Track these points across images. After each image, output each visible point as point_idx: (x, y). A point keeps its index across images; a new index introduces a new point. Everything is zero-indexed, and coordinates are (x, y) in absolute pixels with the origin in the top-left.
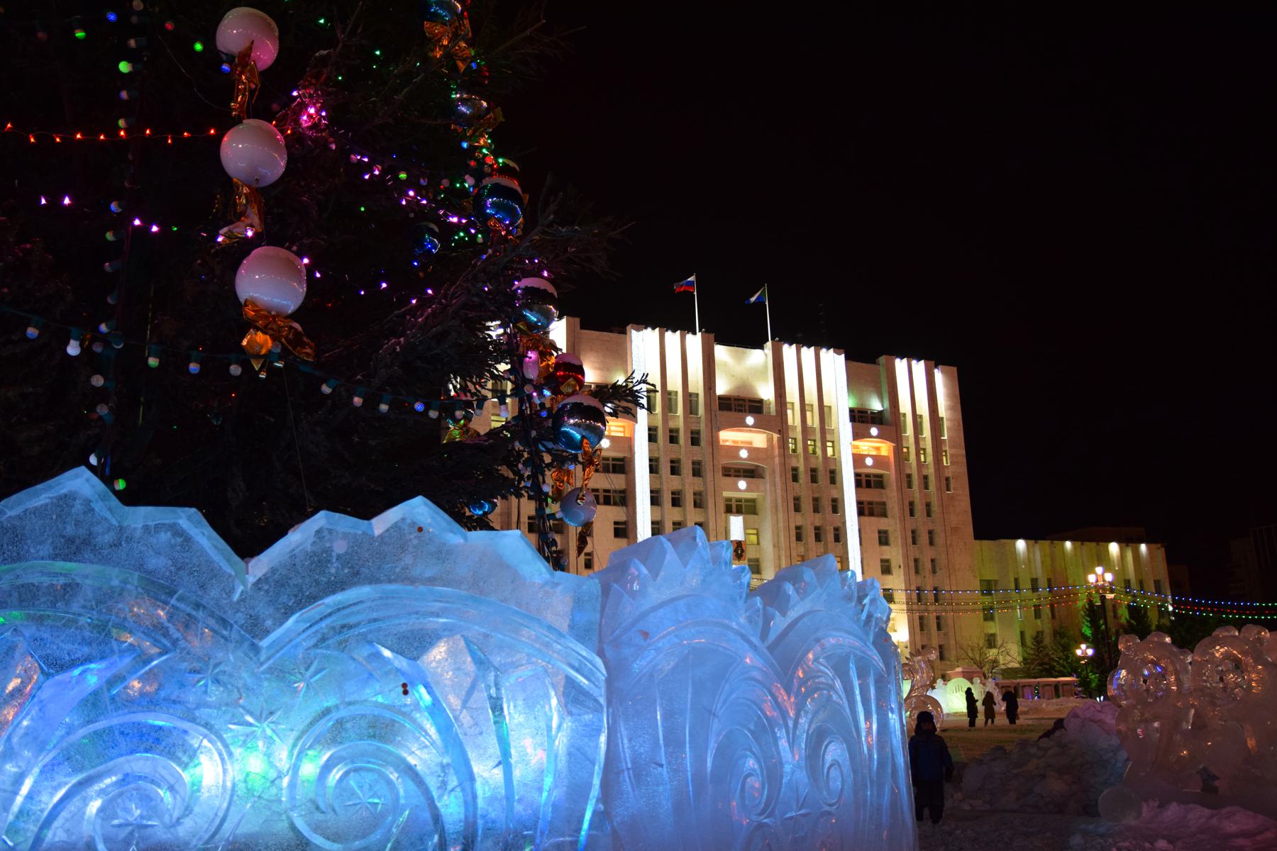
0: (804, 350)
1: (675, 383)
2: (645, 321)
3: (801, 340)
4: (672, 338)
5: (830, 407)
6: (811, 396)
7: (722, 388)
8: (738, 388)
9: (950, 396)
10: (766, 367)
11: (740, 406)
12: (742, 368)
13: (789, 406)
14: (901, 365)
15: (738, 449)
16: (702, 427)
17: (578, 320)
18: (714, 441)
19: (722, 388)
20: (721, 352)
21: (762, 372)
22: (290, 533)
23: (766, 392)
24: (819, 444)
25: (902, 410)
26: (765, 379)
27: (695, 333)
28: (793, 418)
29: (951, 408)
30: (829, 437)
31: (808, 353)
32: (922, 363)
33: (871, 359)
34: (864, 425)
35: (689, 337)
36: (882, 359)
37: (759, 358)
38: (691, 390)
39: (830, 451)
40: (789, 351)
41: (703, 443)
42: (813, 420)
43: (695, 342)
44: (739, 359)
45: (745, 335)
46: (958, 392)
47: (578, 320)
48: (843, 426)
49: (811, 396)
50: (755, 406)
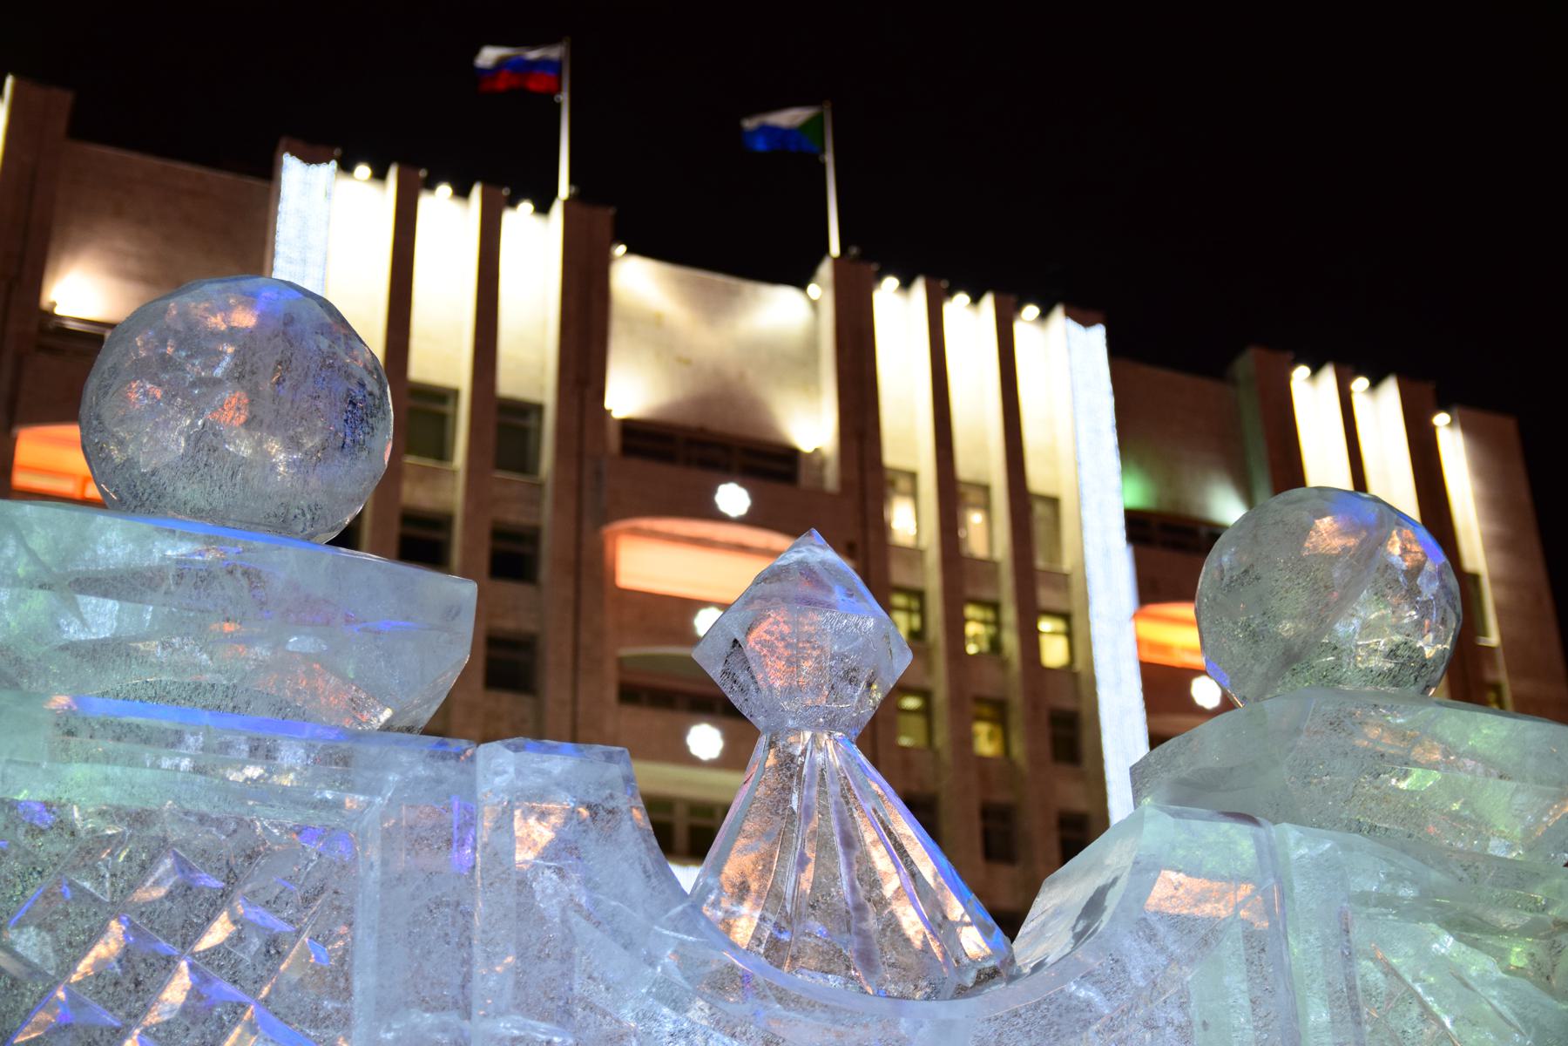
0: (957, 306)
1: (442, 354)
2: (343, 146)
3: (946, 270)
4: (449, 219)
5: (1053, 502)
6: (979, 454)
7: (631, 392)
8: (703, 402)
9: (1496, 503)
10: (812, 345)
11: (697, 452)
12: (673, 332)
13: (973, 496)
14: (1312, 395)
15: (691, 606)
16: (547, 516)
17: (63, 99)
18: (590, 568)
19: (631, 392)
20: (636, 280)
21: (798, 362)
22: (1044, 888)
23: (810, 425)
24: (1009, 615)
25: (893, 456)
26: (809, 383)
27: (543, 208)
28: (909, 521)
29: (1500, 544)
30: (1046, 597)
31: (970, 321)
32: (1390, 391)
33: (1211, 362)
34: (695, 475)
35: (519, 220)
36: (1247, 363)
37: (789, 314)
38: (510, 383)
39: (1054, 652)
40: (897, 309)
41: (545, 571)
42: (986, 534)
43: (535, 241)
44: (714, 309)
45: (743, 238)
46: (1524, 496)
47: (63, 99)
48: (1104, 562)
49: (979, 454)
50: (770, 465)
